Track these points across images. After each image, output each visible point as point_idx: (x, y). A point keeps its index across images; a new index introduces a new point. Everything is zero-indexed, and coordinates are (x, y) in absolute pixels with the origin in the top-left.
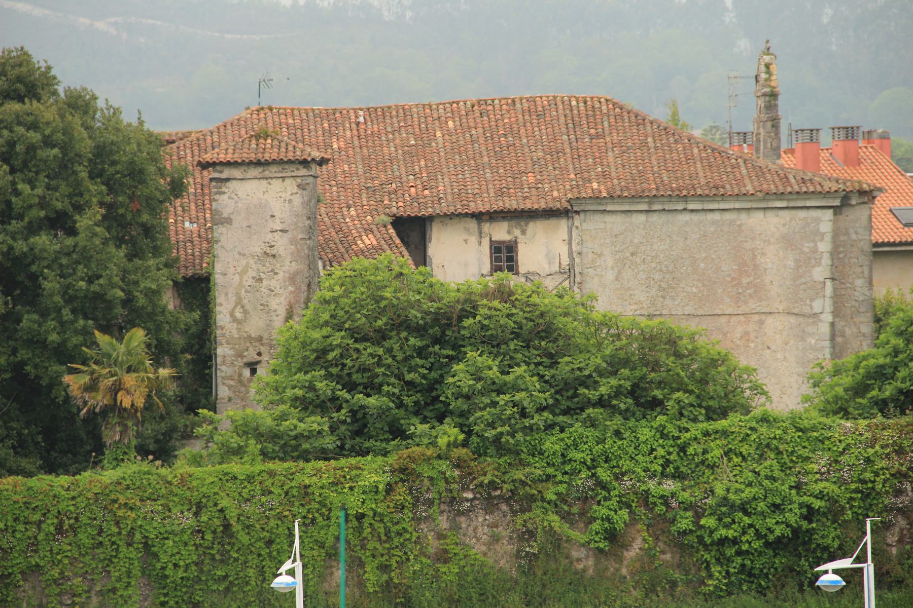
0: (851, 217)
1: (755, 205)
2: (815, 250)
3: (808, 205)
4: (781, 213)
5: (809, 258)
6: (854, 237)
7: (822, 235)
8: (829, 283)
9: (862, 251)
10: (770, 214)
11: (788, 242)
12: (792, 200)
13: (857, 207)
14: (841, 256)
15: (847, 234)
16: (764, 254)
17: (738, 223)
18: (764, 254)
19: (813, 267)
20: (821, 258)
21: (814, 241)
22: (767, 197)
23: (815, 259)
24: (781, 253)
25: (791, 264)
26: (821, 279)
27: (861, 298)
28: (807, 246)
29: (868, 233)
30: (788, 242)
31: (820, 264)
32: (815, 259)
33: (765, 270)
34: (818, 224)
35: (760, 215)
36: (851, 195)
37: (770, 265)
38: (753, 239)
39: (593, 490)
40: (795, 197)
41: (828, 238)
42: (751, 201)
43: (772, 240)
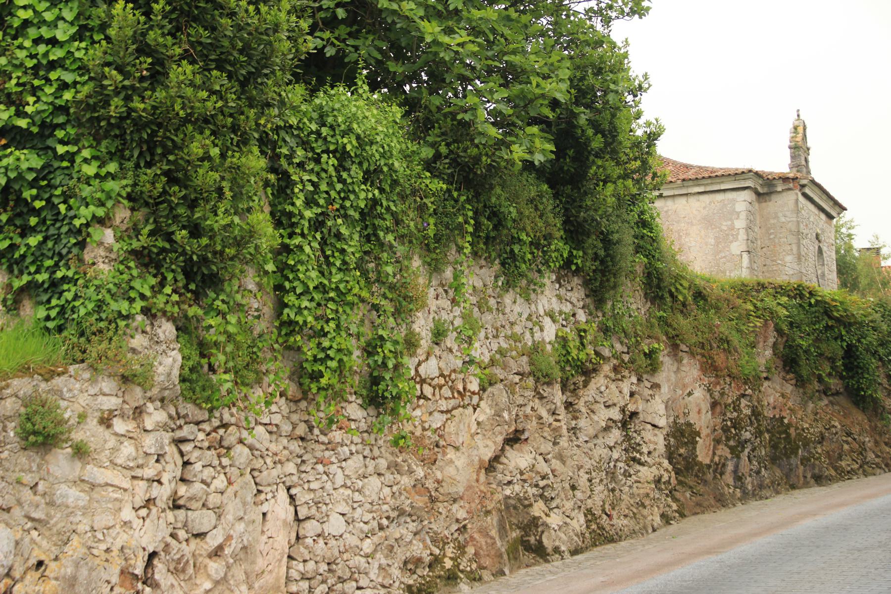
0: (779, 202)
1: (677, 192)
2: (732, 228)
3: (723, 188)
4: (702, 197)
5: (727, 235)
6: (783, 219)
7: (738, 213)
8: (745, 255)
9: (790, 231)
10: (692, 200)
11: (708, 222)
12: (707, 184)
13: (784, 194)
14: (772, 237)
15: (777, 217)
16: (687, 234)
17: (665, 209)
18: (687, 234)
19: (731, 242)
20: (738, 234)
21: (731, 220)
22: (686, 183)
23: (732, 235)
24: (703, 232)
25: (712, 241)
26: (739, 253)
27: (791, 272)
28: (725, 225)
29: (795, 215)
30: (708, 222)
31: (737, 240)
32: (732, 235)
33: (689, 248)
34: (734, 205)
35: (683, 200)
36: (775, 182)
37: (693, 244)
38: (678, 222)
39: (366, 227)
40: (709, 181)
41: (743, 216)
42: (673, 188)
43: (694, 221)
